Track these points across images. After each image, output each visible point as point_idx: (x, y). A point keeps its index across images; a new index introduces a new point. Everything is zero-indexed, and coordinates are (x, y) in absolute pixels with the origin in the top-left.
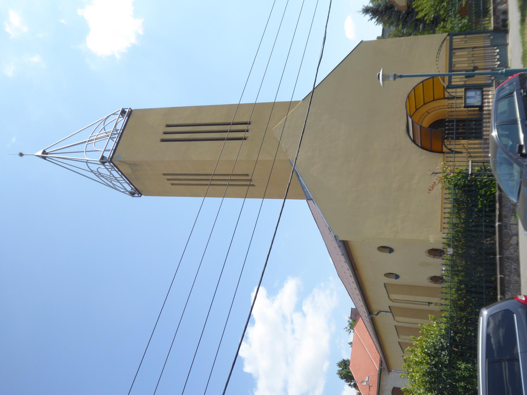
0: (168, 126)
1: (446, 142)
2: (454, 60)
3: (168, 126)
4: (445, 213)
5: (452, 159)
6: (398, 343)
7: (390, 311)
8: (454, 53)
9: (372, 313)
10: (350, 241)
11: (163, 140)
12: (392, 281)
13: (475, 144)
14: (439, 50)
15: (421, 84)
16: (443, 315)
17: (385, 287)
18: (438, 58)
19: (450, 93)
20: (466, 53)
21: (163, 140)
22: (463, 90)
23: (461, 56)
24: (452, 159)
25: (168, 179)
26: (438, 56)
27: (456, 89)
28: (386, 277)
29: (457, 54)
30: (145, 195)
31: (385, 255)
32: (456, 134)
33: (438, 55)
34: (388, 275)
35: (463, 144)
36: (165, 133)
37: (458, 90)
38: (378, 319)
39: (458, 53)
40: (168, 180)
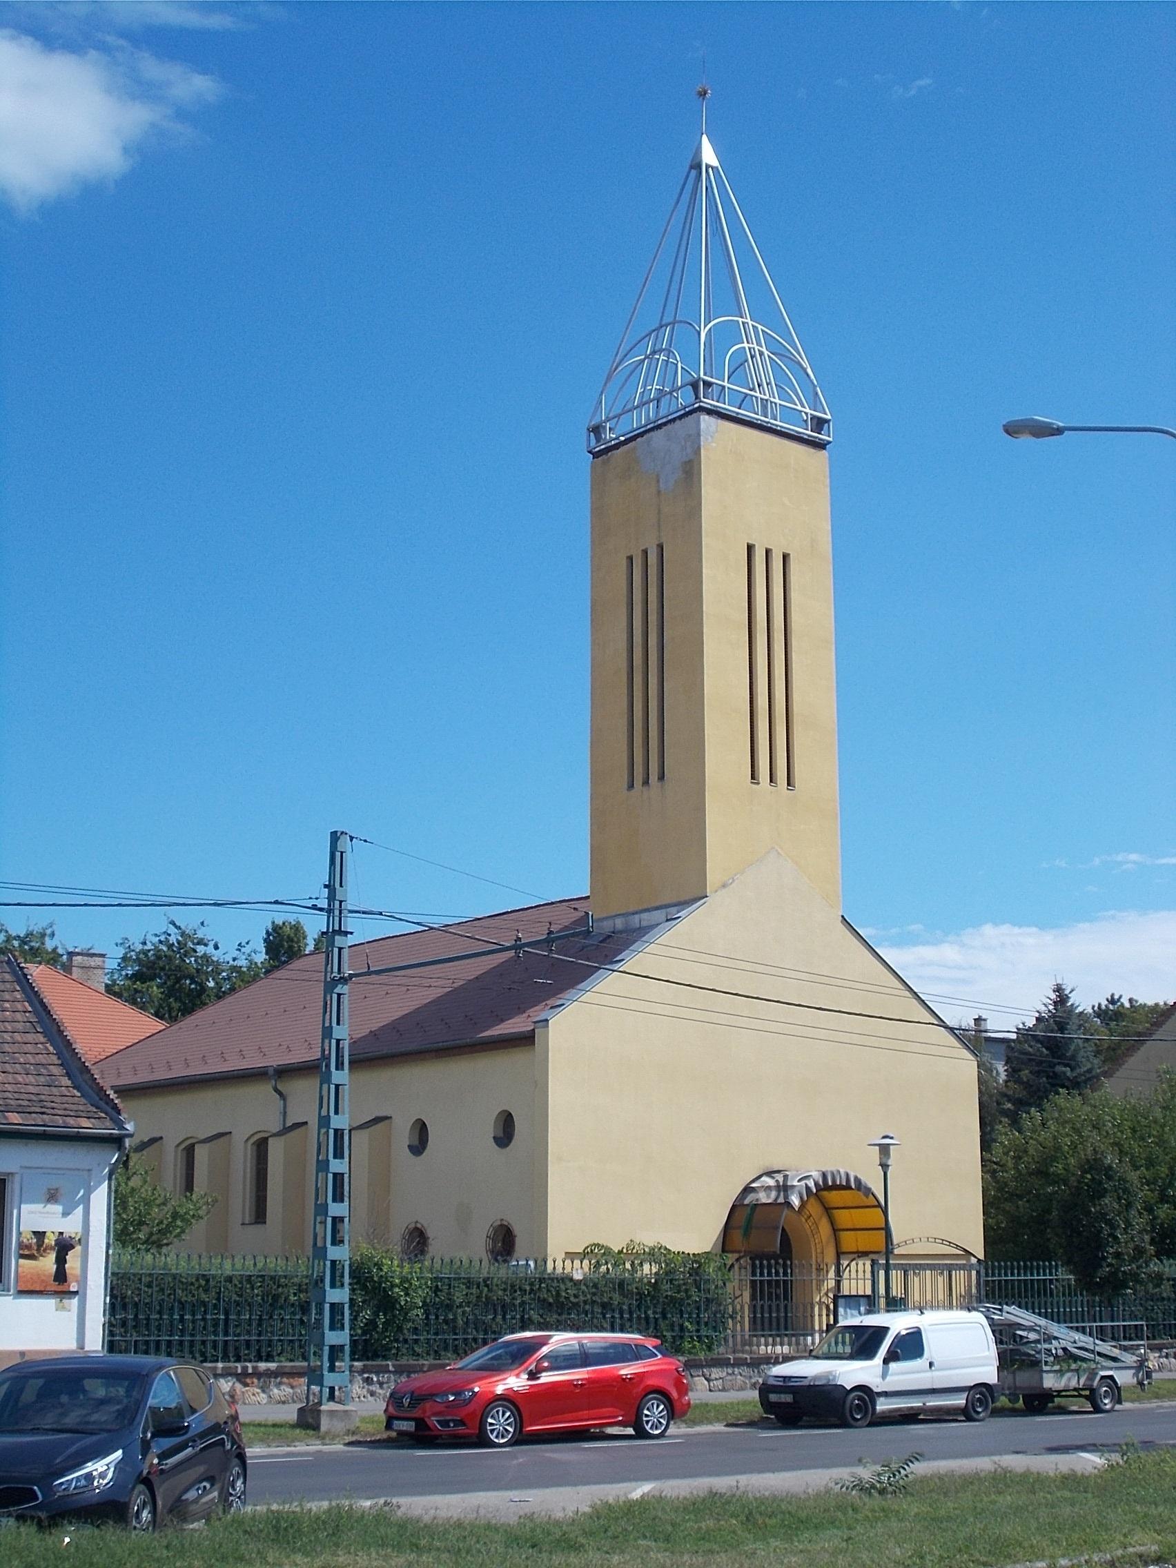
0: (785, 557)
1: (745, 1261)
2: (928, 1272)
3: (785, 557)
4: (554, 1262)
5: (861, 1275)
6: (157, 1135)
7: (289, 1124)
8: (942, 1273)
9: (279, 1077)
10: (534, 1049)
11: (750, 548)
12: (402, 1134)
13: (820, 1315)
14: (950, 1242)
15: (876, 1204)
16: (532, 1263)
17: (378, 1120)
18: (933, 1240)
19: (848, 1268)
20: (941, 1297)
21: (750, 548)
22: (869, 1292)
23: (935, 1291)
24: (861, 1275)
25: (647, 553)
26: (937, 1241)
27: (82, 1257)
28: (495, 1142)
29: (940, 1279)
30: (593, 467)
31: (488, 1129)
32: (784, 1280)
33: (941, 1241)
34: (422, 1130)
35: (742, 1295)
36: (768, 552)
37: (869, 1283)
38: (264, 1091)
39: (941, 1281)
40: (645, 552)
